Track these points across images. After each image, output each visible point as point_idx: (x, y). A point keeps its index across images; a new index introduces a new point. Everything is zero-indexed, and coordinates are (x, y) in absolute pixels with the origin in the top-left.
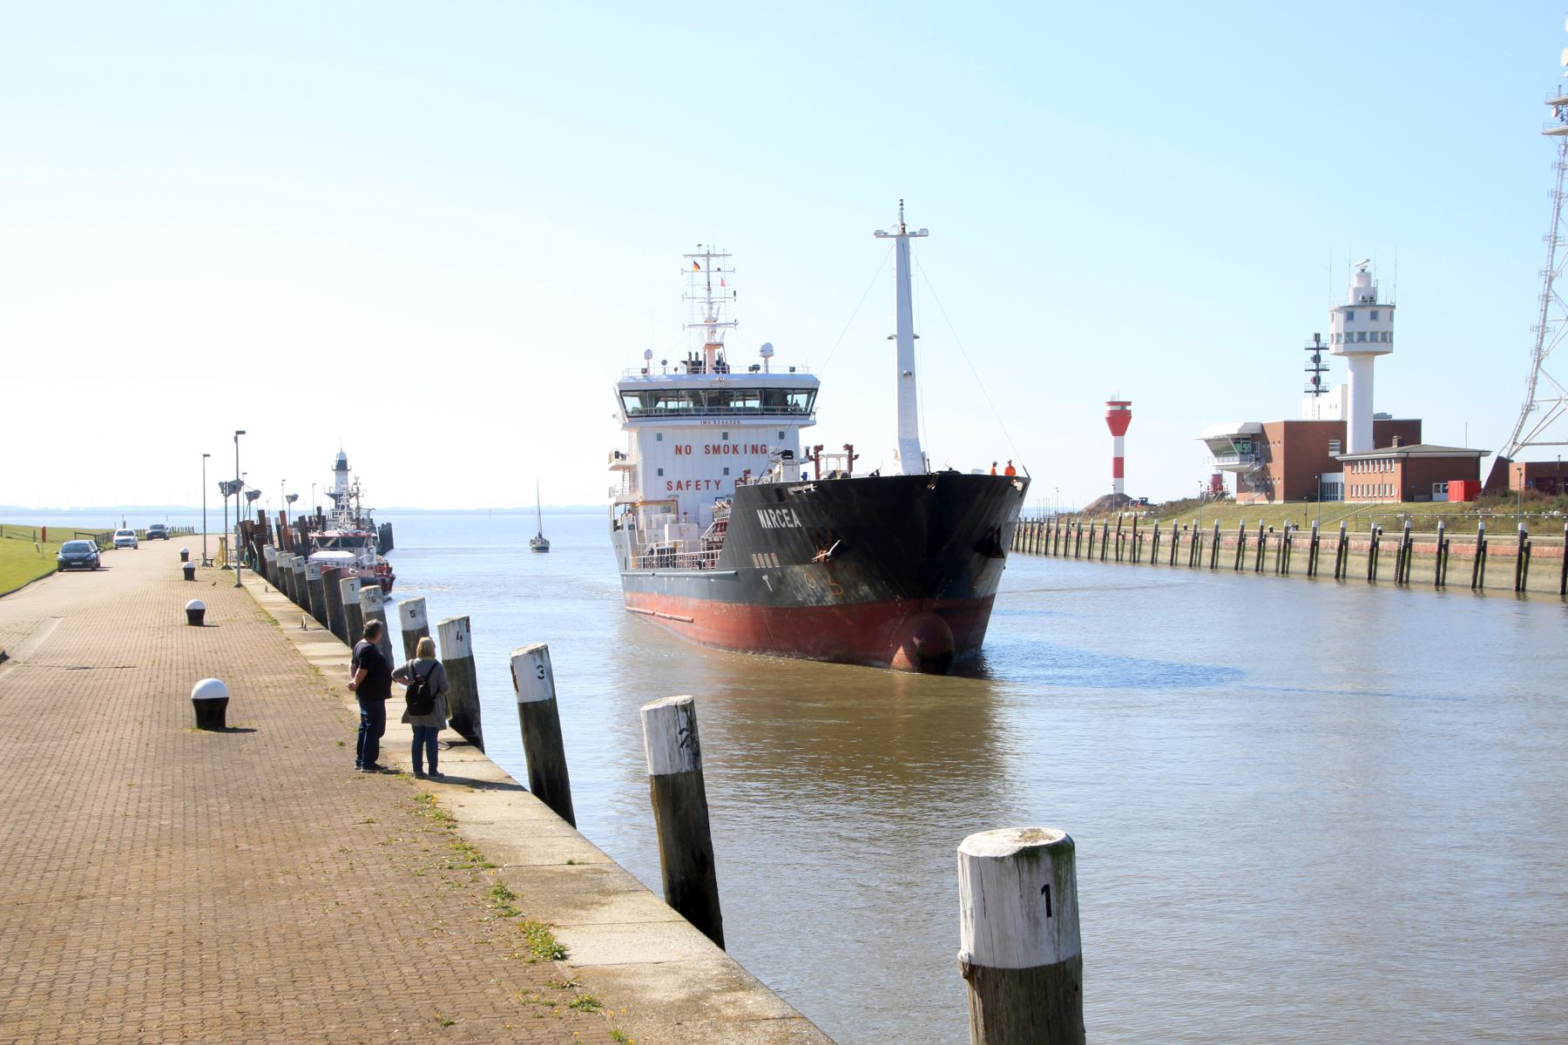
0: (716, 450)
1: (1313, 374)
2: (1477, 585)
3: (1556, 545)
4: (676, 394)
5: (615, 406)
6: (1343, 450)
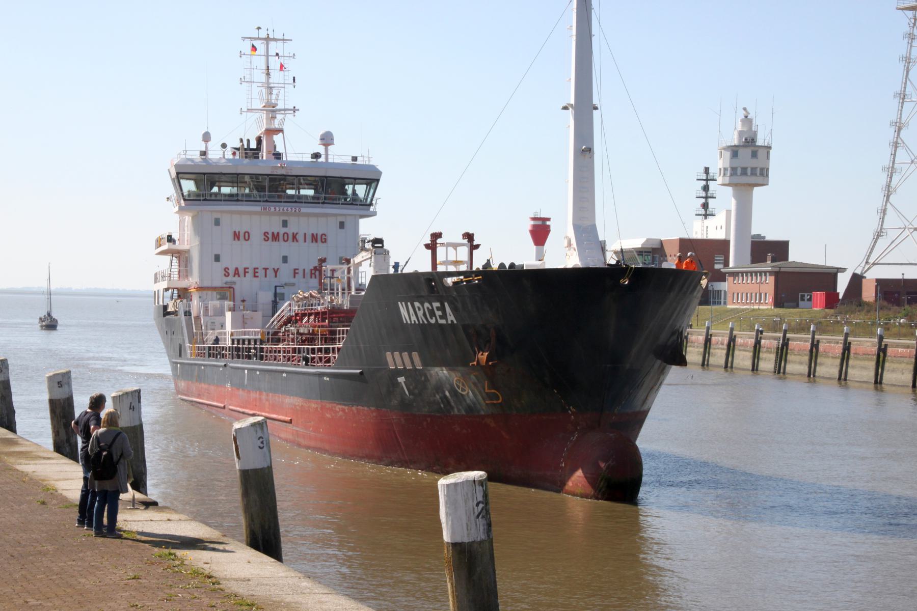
0: (275, 237)
1: (703, 200)
2: (842, 378)
3: (908, 347)
4: (235, 179)
5: (171, 191)
6: (726, 264)
